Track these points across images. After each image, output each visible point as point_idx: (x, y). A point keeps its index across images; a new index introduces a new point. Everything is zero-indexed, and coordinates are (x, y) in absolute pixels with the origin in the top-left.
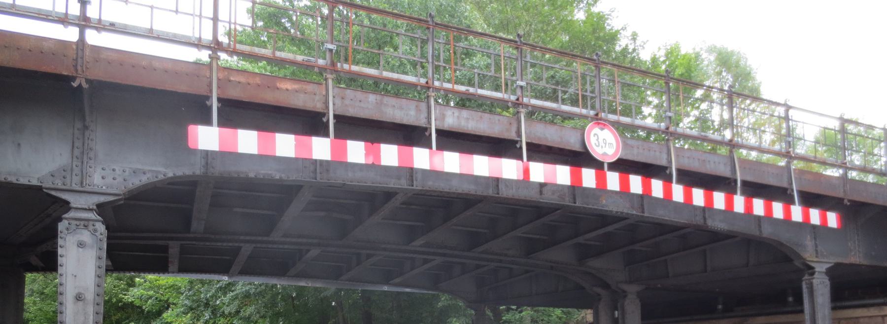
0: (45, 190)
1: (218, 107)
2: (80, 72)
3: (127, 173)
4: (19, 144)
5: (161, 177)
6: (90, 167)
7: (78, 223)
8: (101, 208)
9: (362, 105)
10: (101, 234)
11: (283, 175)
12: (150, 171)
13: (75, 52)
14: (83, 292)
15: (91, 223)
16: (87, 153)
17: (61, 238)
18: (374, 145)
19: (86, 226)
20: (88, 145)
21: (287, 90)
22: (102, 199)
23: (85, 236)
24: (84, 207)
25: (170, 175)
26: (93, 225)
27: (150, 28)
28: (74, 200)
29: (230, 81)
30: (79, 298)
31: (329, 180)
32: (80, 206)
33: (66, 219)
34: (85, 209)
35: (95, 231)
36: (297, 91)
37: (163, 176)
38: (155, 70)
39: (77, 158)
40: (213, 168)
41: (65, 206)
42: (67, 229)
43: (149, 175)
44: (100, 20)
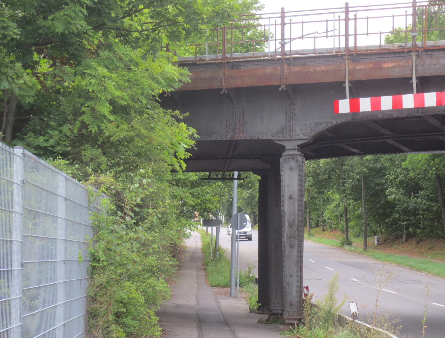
0: (274, 141)
1: (349, 86)
2: (282, 82)
3: (312, 126)
4: (263, 118)
5: (330, 125)
6: (295, 125)
7: (289, 157)
8: (301, 147)
9: (436, 67)
10: (300, 162)
11: (399, 114)
12: (324, 122)
13: (280, 72)
14: (293, 194)
15: (295, 156)
16: (293, 118)
17: (282, 166)
18: (442, 93)
19: (293, 159)
20: (293, 113)
21: (388, 67)
22: (300, 142)
23: (293, 164)
24: (291, 148)
25: (335, 123)
26: (296, 158)
27: (313, 48)
28: (288, 145)
29: (356, 70)
30: (291, 198)
31: (434, 112)
32: (289, 148)
33: (284, 155)
34: (292, 149)
35: (297, 160)
36: (394, 67)
37: (330, 124)
38: (317, 72)
39: (289, 121)
40: (358, 115)
41: (283, 149)
42: (284, 161)
43: (324, 125)
44: (291, 51)
